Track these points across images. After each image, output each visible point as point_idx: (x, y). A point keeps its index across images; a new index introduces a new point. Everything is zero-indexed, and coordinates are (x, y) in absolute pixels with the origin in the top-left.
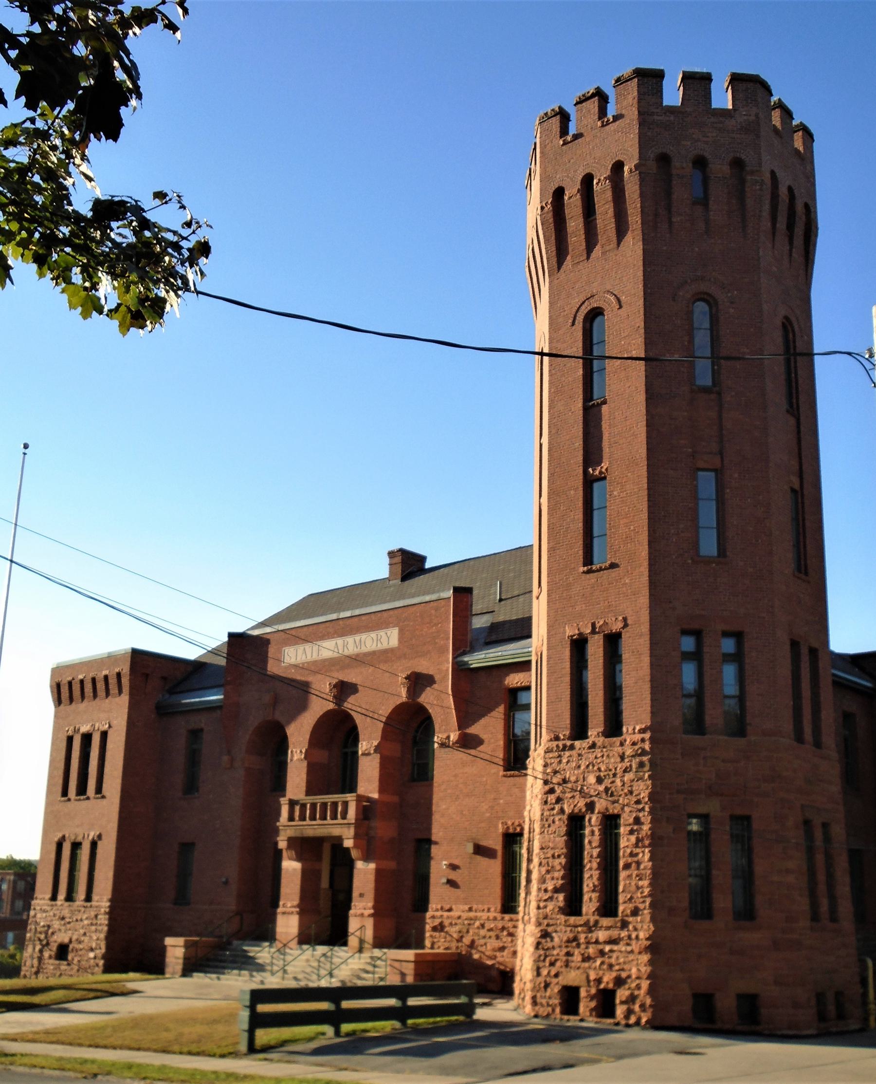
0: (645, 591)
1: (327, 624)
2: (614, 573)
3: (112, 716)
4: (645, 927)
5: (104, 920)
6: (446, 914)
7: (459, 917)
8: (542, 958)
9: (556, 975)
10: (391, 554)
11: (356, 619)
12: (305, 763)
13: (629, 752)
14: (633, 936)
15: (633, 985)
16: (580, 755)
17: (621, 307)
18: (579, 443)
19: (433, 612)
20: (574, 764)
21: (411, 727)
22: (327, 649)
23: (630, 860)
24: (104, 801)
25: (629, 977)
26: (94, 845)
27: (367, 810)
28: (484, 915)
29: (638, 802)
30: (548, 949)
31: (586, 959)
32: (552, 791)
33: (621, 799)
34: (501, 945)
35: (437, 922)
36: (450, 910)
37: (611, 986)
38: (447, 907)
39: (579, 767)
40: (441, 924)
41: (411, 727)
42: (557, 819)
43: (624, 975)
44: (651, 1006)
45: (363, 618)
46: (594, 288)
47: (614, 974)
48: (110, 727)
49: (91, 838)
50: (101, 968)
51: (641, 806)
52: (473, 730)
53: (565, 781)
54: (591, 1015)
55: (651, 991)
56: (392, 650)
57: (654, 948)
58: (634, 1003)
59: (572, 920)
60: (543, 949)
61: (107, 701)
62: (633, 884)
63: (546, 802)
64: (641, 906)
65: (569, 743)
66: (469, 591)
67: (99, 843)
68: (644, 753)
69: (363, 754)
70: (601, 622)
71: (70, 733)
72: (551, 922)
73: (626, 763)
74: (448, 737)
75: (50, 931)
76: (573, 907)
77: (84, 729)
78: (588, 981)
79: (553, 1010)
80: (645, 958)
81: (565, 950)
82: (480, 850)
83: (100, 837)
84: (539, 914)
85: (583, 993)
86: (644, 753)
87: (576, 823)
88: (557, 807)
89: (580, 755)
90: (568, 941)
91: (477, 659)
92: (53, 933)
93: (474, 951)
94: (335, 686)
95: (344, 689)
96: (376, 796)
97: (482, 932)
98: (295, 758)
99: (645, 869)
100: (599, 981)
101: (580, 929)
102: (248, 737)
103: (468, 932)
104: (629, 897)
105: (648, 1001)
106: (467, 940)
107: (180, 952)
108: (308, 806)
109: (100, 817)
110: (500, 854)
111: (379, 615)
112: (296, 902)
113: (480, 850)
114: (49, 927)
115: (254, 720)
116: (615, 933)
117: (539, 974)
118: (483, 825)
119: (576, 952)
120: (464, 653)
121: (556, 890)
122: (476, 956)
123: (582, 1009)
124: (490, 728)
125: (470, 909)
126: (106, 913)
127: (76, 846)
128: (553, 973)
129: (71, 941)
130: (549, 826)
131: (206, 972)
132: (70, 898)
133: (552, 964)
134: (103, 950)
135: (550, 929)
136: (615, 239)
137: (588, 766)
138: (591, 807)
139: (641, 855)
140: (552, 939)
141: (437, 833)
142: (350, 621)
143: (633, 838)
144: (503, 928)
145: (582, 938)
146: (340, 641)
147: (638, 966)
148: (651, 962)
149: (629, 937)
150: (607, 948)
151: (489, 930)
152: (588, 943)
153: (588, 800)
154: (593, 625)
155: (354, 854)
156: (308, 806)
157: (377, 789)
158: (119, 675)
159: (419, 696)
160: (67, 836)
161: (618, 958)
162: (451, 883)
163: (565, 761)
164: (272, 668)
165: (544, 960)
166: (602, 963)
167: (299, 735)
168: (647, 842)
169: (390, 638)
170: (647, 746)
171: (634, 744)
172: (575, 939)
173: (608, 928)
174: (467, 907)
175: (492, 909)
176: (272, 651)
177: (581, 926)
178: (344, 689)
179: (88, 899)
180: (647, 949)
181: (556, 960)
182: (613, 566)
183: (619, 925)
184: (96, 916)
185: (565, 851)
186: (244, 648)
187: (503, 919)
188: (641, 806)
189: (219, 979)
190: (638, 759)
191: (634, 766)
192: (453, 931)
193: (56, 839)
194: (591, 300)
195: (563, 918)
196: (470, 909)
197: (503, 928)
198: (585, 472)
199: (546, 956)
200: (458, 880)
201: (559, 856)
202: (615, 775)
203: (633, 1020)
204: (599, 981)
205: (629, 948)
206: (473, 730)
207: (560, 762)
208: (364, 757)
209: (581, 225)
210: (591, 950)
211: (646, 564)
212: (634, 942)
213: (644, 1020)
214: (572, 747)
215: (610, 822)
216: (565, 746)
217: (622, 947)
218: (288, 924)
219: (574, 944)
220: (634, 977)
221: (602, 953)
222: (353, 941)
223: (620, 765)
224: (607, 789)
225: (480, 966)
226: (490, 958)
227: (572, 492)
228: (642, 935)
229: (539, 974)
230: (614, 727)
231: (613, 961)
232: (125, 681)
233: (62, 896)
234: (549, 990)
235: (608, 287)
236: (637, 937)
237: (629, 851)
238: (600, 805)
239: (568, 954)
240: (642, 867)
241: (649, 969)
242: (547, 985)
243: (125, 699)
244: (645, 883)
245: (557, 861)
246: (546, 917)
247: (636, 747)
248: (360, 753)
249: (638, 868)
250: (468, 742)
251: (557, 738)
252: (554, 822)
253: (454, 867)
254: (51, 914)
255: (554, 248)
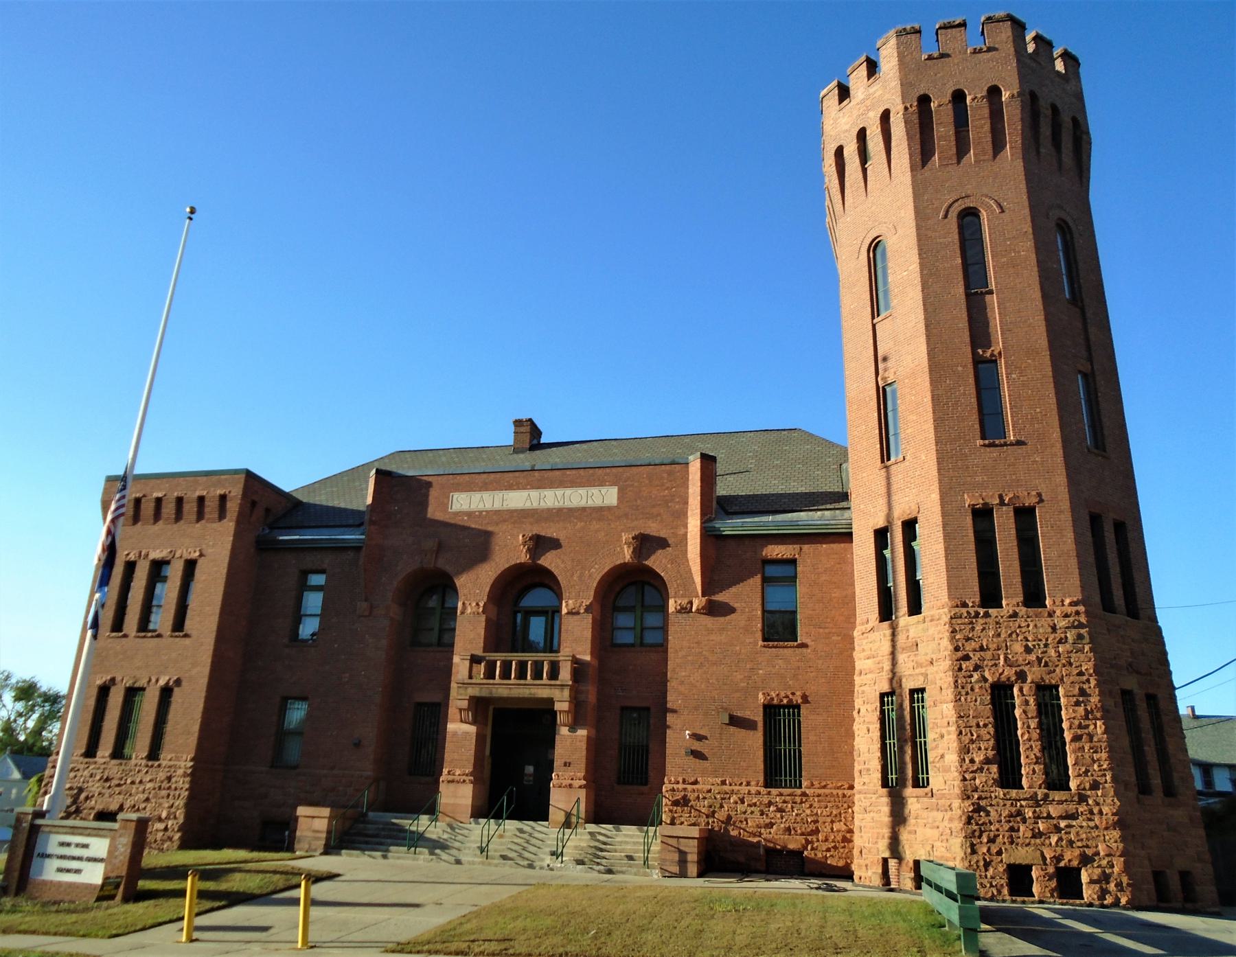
0: (1061, 470)
1: (517, 474)
2: (1020, 450)
3: (214, 546)
4: (1109, 801)
5: (182, 784)
6: (689, 787)
7: (709, 791)
8: (977, 834)
9: (999, 853)
10: (518, 423)
11: (557, 473)
12: (483, 618)
13: (1062, 623)
14: (1096, 810)
15: (1104, 862)
16: (997, 623)
17: (1003, 211)
18: (963, 323)
19: (665, 475)
20: (991, 633)
21: (633, 589)
22: (517, 499)
23: (1079, 732)
24: (187, 641)
25: (1097, 854)
26: (166, 692)
27: (579, 670)
28: (744, 789)
29: (1081, 674)
30: (984, 824)
31: (1037, 835)
32: (966, 658)
33: (1058, 670)
34: (768, 821)
35: (679, 796)
36: (696, 783)
37: (1075, 863)
38: (693, 779)
39: (999, 635)
40: (684, 797)
41: (633, 589)
42: (977, 687)
43: (1089, 852)
44: (1128, 885)
45: (568, 472)
46: (969, 189)
47: (1077, 852)
48: (201, 555)
49: (162, 682)
50: (176, 844)
51: (1085, 678)
52: (720, 597)
53: (982, 649)
54: (1052, 896)
55: (1127, 869)
56: (609, 508)
57: (1120, 823)
58: (1108, 883)
59: (1014, 793)
60: (977, 824)
61: (198, 525)
62: (1087, 756)
63: (960, 669)
64: (1102, 780)
65: (982, 611)
66: (713, 459)
67: (176, 690)
68: (1081, 625)
69: (568, 613)
70: (1011, 495)
71: (132, 557)
72: (983, 795)
73: (1059, 635)
74: (691, 603)
75: (83, 796)
76: (1009, 777)
77: (156, 555)
78: (1044, 858)
79: (999, 892)
80: (1116, 834)
81: (1007, 826)
82: (735, 721)
83: (178, 682)
84: (965, 786)
85: (1034, 874)
86: (1081, 625)
87: (1001, 694)
88: (976, 676)
89: (997, 623)
90: (1011, 815)
91: (731, 526)
92: (87, 798)
93: (730, 828)
94: (531, 539)
95: (540, 544)
96: (588, 658)
97: (740, 807)
98: (469, 610)
99: (1099, 741)
100: (1058, 859)
101: (1023, 803)
102: (395, 583)
103: (722, 806)
104: (1083, 769)
105: (1125, 880)
106: (721, 815)
107: (322, 825)
108: (498, 663)
109: (185, 661)
110: (760, 725)
111: (591, 471)
112: (469, 769)
113: (735, 721)
114: (81, 790)
115: (405, 567)
116: (1071, 808)
117: (974, 852)
118: (738, 695)
119: (1022, 828)
120: (710, 520)
121: (987, 761)
122: (734, 833)
123: (1036, 889)
124: (746, 596)
125: (724, 783)
126: (185, 775)
127: (132, 693)
128: (994, 850)
129: (121, 808)
130: (967, 694)
131: (363, 850)
132: (118, 753)
133: (992, 840)
134: (181, 820)
135: (983, 803)
136: (990, 152)
137: (1010, 635)
138: (1021, 676)
139: (1092, 727)
140: (988, 814)
141: (673, 700)
142: (550, 473)
143: (1081, 710)
144: (770, 804)
145: (1029, 813)
146: (534, 494)
147: (1109, 842)
148: (1123, 839)
149: (1091, 812)
150: (1063, 824)
151: (750, 805)
152: (1037, 817)
153: (1018, 669)
154: (1001, 497)
155: (561, 718)
156: (498, 663)
157: (589, 651)
158: (223, 498)
159: (647, 558)
160: (118, 679)
161: (1077, 833)
162: (697, 755)
163: (978, 628)
164: (433, 512)
165: (980, 837)
166: (1060, 839)
167: (473, 592)
168: (1098, 715)
169: (608, 496)
170: (1083, 619)
171: (1066, 616)
172: (1019, 813)
173: (1060, 802)
174: (719, 780)
175: (753, 783)
176: (433, 493)
177: (1025, 799)
178: (540, 544)
179: (154, 754)
180: (1115, 825)
181: (996, 836)
182: (1019, 443)
183: (1076, 798)
184: (169, 779)
185: (991, 720)
186: (399, 489)
187: (769, 793)
188: (1085, 678)
189: (385, 857)
190: (1074, 631)
191: (1070, 640)
192: (703, 806)
193: (99, 682)
194: (966, 200)
195: (1000, 792)
196: (724, 783)
197: (770, 804)
198: (974, 353)
199: (981, 832)
200: (705, 751)
201: (985, 726)
202: (1046, 645)
203: (1109, 900)
204: (1058, 859)
205: (1092, 824)
206: (720, 597)
207: (973, 629)
208: (570, 617)
209: (952, 132)
210: (1041, 826)
211: (1059, 445)
212: (1097, 818)
213: (1123, 901)
214: (987, 615)
215: (1046, 695)
216: (977, 614)
217: (1080, 821)
218: (457, 794)
219: (1018, 819)
220: (1102, 853)
221: (1058, 829)
222: (556, 815)
223: (1052, 636)
224: (1039, 660)
225: (740, 844)
226: (755, 835)
227: (960, 369)
228: (1105, 810)
229: (974, 852)
230: (1034, 596)
231: (1072, 837)
232: (233, 507)
233: (105, 751)
234: (991, 870)
235: (985, 191)
236: (1101, 812)
237: (1076, 722)
238: (1033, 674)
239: (1012, 829)
240: (1095, 739)
241: (1121, 846)
242: (987, 865)
243: (229, 525)
244: (1104, 755)
245: (983, 732)
246: (976, 790)
247: (1071, 619)
248: (564, 611)
249: (1091, 741)
250: (714, 609)
251: (964, 605)
252: (972, 689)
253: (698, 737)
254: (86, 773)
255: (918, 147)
